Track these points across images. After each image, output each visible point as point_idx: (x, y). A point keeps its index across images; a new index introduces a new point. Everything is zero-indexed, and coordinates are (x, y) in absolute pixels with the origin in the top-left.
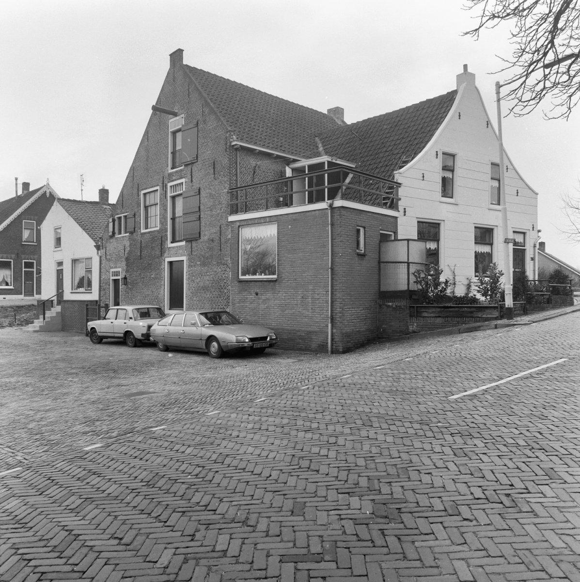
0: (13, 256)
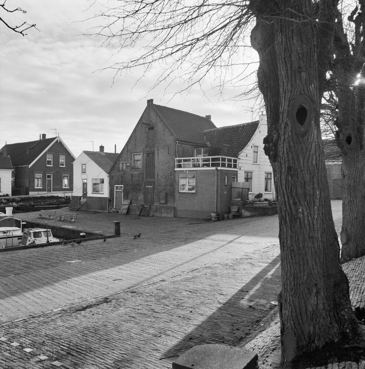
0: (42, 172)
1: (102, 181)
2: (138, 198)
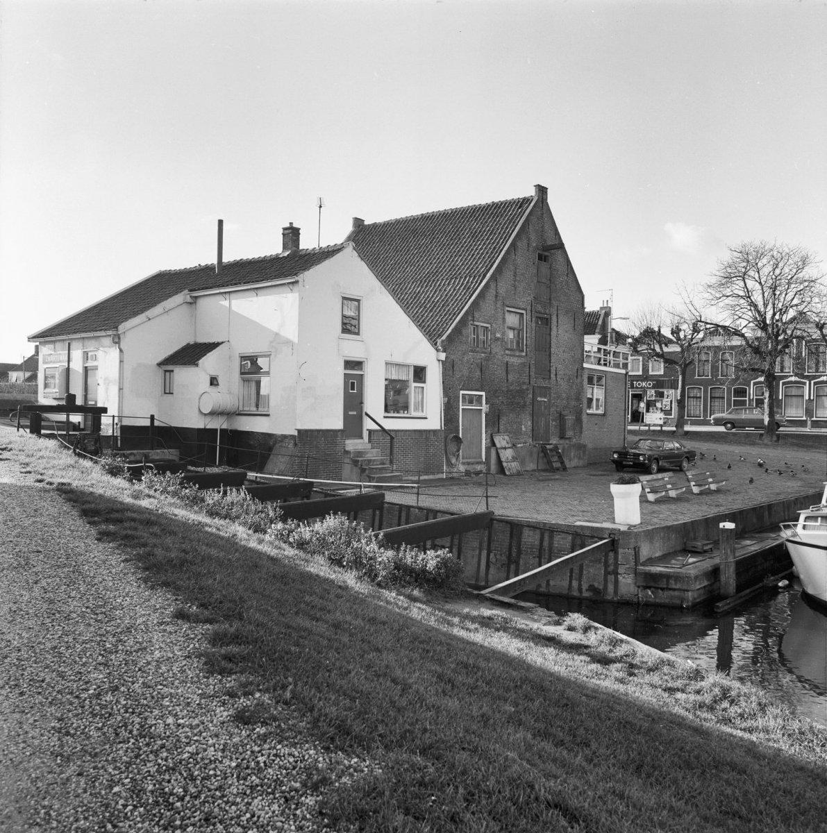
1: (420, 373)
2: (521, 429)
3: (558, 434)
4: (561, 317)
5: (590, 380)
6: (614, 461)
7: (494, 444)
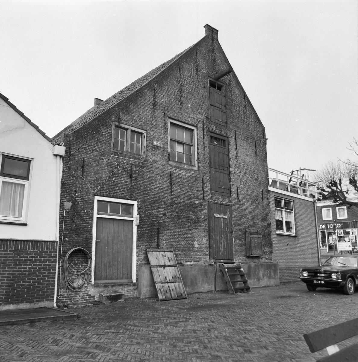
2: (193, 245)
3: (244, 253)
4: (239, 143)
5: (278, 203)
6: (304, 280)
7: (148, 262)
